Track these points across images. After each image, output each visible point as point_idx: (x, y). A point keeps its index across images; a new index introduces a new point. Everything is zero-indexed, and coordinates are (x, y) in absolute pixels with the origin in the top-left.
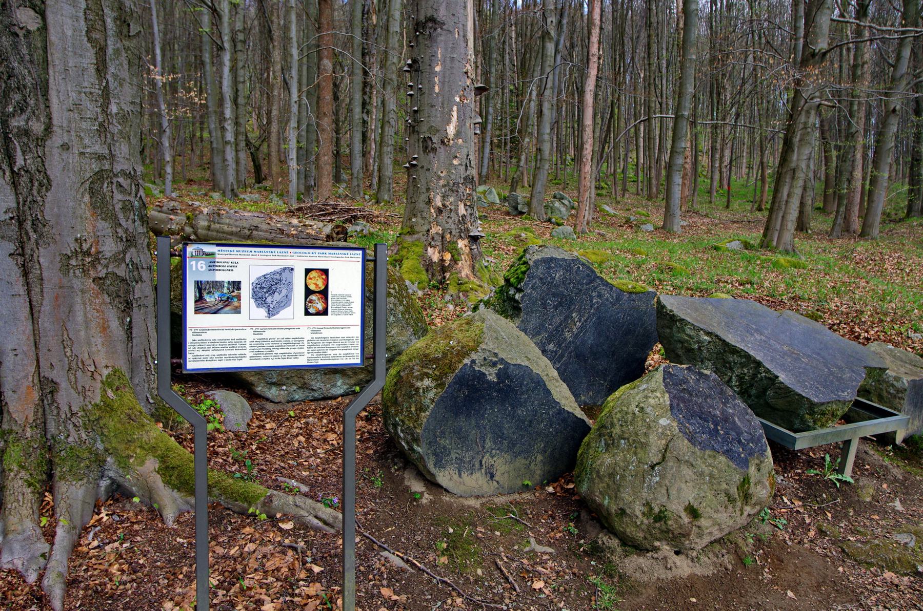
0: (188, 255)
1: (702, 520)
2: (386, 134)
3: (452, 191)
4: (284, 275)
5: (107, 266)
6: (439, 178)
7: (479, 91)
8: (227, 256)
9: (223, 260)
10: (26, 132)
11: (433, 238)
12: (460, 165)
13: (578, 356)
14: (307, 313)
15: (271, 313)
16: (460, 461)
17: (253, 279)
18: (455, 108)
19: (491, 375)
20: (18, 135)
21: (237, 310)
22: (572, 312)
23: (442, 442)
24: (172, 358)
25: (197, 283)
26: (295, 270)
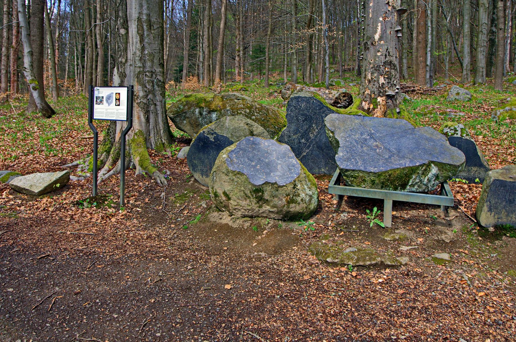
1: (232, 201)
2: (480, 39)
3: (376, 70)
5: (140, 99)
6: (370, 63)
7: (401, 12)
10: (121, 62)
11: (365, 97)
12: (381, 55)
13: (318, 147)
14: (116, 105)
15: (109, 105)
16: (202, 170)
18: (379, 24)
19: (212, 138)
20: (120, 63)
21: (103, 104)
22: (312, 124)
23: (194, 161)
25: (96, 97)
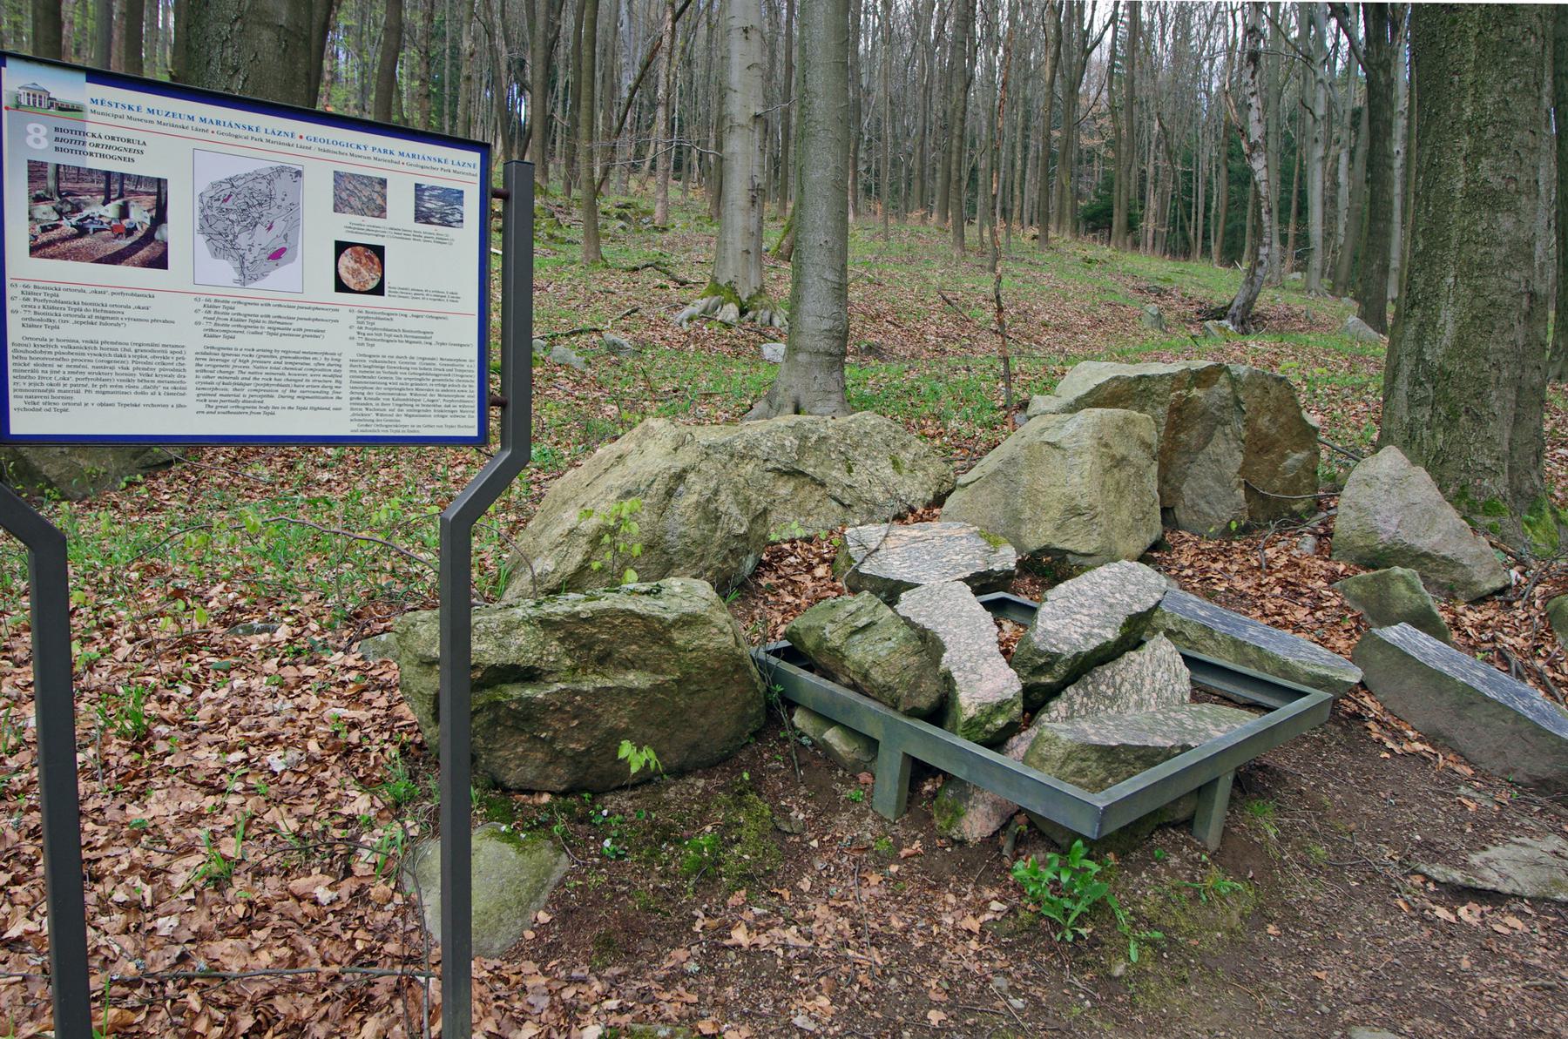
0: (5, 103)
4: (281, 185)
8: (118, 122)
9: (104, 131)
17: (203, 186)
24: (1363, 4)
26: (305, 174)
